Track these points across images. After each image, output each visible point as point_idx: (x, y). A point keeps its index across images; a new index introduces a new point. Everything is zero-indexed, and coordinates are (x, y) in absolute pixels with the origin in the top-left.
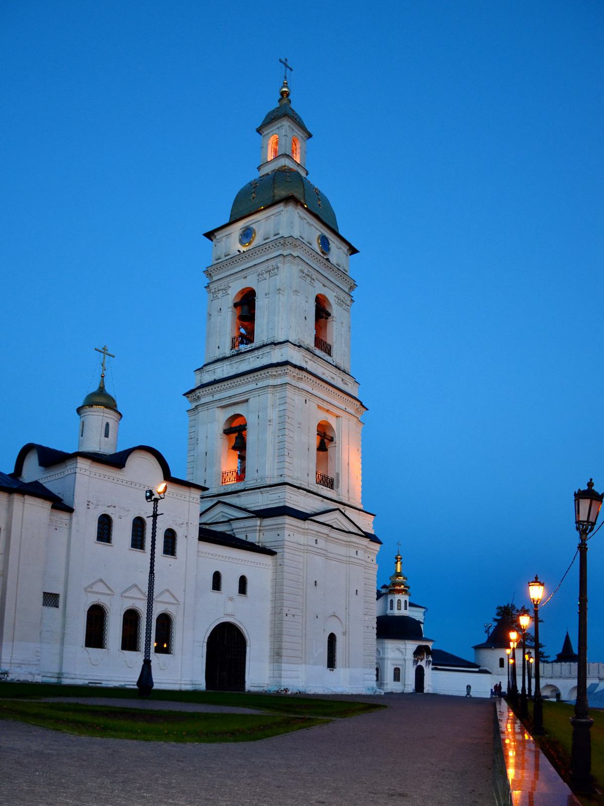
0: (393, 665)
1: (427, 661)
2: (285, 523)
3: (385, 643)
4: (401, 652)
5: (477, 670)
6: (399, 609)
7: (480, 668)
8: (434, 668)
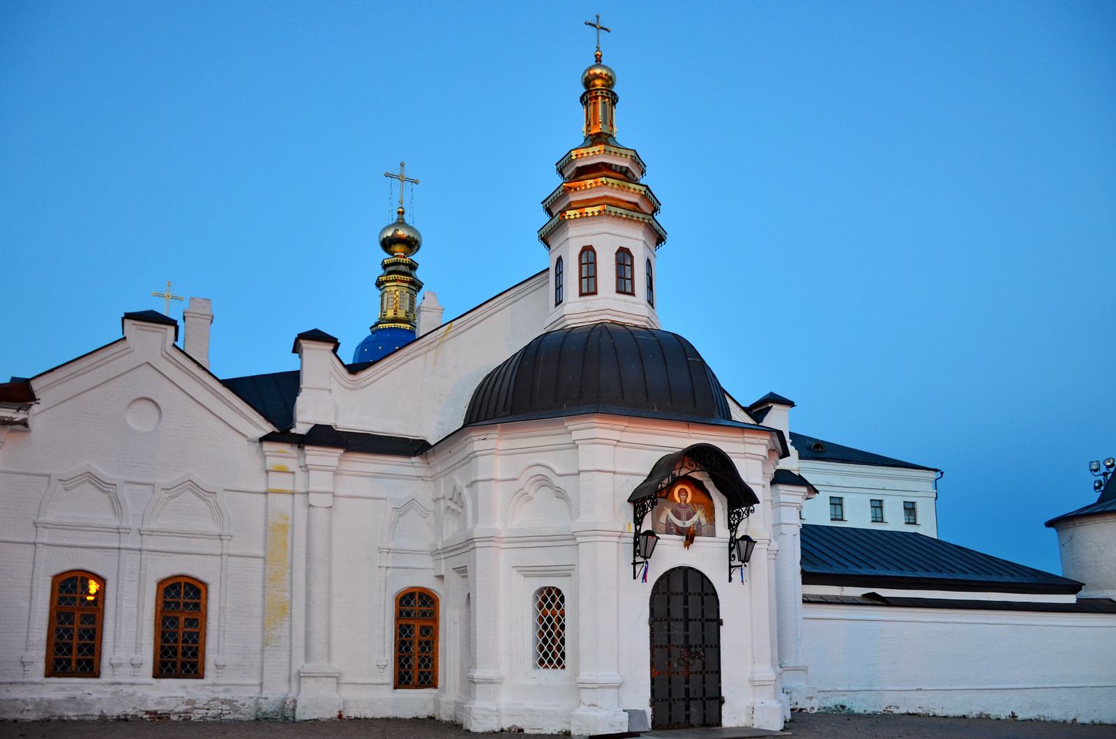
0: (528, 571)
1: (733, 542)
2: (564, 315)
3: (473, 456)
4: (561, 494)
5: (1071, 599)
6: (589, 287)
7: (1083, 594)
8: (866, 596)
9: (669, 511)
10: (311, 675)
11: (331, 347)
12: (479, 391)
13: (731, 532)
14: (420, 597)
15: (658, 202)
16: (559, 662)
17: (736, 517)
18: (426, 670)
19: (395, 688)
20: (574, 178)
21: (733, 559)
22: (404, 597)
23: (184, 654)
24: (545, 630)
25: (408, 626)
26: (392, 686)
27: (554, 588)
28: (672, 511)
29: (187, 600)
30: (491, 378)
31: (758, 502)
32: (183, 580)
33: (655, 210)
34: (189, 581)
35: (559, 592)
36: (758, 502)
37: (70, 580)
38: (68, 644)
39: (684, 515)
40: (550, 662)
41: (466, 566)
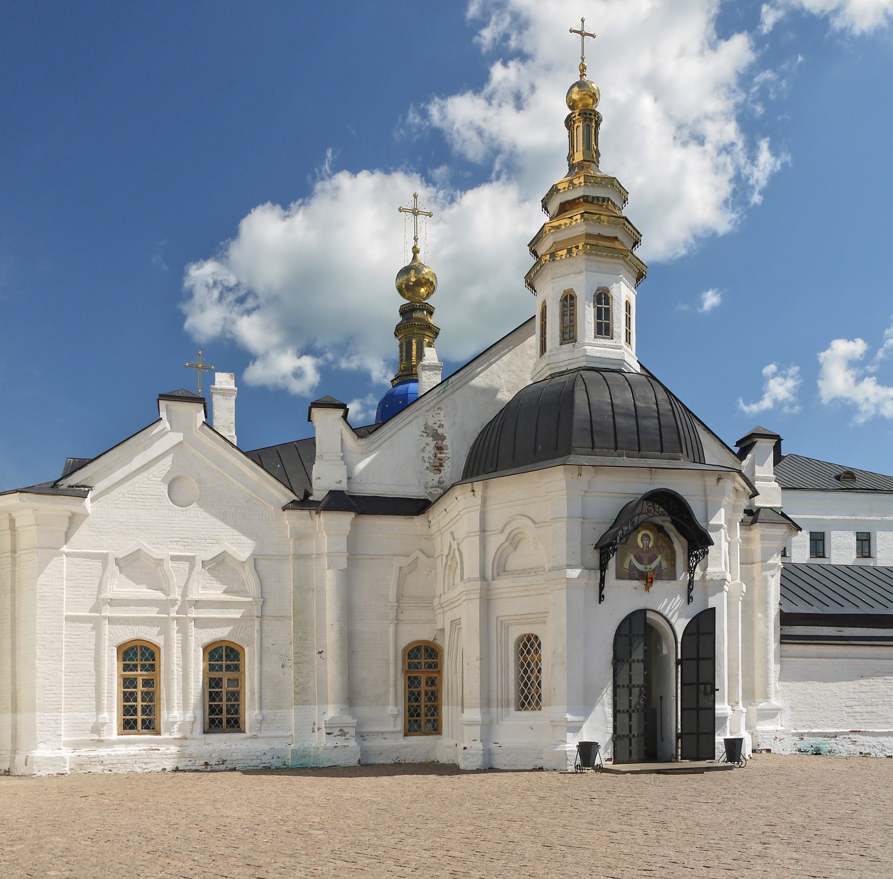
6: (569, 335)
9: (632, 557)
10: (333, 725)
11: (341, 412)
12: (474, 446)
13: (690, 573)
14: (426, 650)
15: (638, 233)
16: (537, 704)
17: (694, 559)
18: (432, 718)
19: (405, 735)
20: (557, 215)
21: (602, 599)
22: (412, 650)
23: (228, 712)
24: (525, 675)
25: (416, 678)
26: (402, 734)
27: (533, 635)
28: (635, 557)
29: (229, 663)
30: (484, 433)
31: (713, 544)
32: (139, 644)
33: (636, 243)
34: (215, 647)
35: (536, 638)
36: (713, 544)
37: (132, 648)
38: (134, 706)
39: (646, 560)
40: (529, 703)
41: (460, 618)
